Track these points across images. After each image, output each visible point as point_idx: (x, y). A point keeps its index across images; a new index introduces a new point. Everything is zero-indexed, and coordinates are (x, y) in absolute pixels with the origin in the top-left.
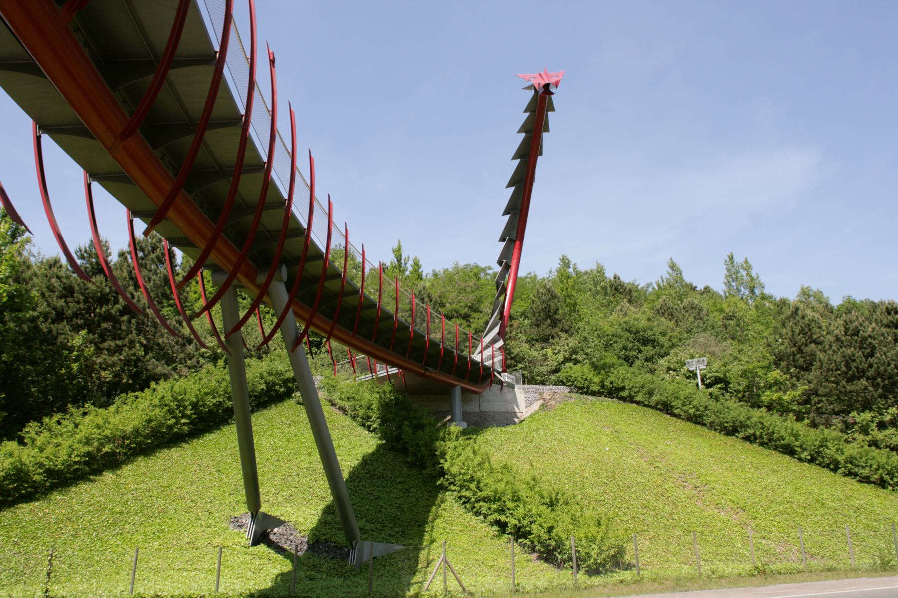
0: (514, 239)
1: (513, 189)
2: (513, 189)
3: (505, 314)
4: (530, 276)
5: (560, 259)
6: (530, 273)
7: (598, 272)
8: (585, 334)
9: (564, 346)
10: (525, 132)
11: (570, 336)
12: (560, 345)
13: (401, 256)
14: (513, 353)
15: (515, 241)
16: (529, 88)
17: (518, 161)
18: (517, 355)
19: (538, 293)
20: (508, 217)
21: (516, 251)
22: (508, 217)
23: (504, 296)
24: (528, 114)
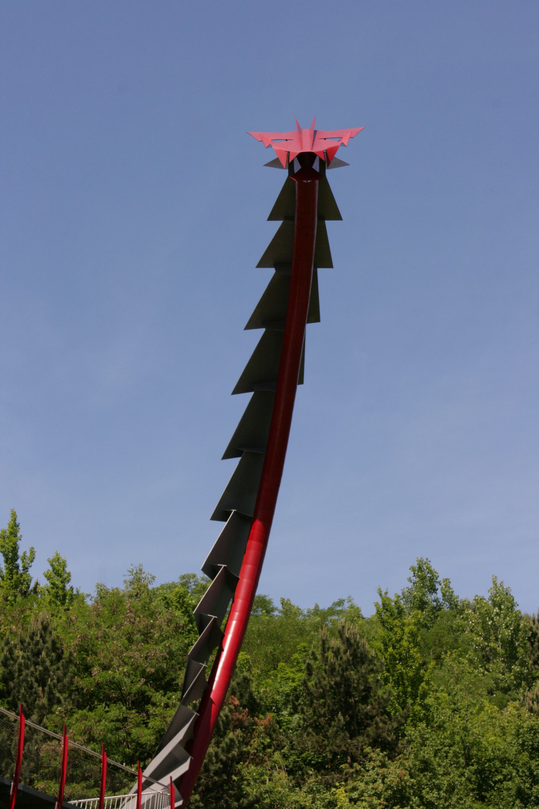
0: (251, 515)
1: (247, 397)
2: (247, 397)
3: (212, 696)
4: (339, 608)
5: (413, 569)
6: (340, 603)
7: (495, 604)
8: (427, 753)
9: (375, 781)
10: (276, 265)
11: (391, 758)
12: (366, 778)
13: (15, 549)
14: (247, 795)
15: (252, 521)
16: (275, 163)
17: (260, 332)
18: (258, 800)
19: (324, 650)
20: (235, 462)
21: (253, 546)
22: (235, 462)
23: (215, 652)
24: (277, 224)
